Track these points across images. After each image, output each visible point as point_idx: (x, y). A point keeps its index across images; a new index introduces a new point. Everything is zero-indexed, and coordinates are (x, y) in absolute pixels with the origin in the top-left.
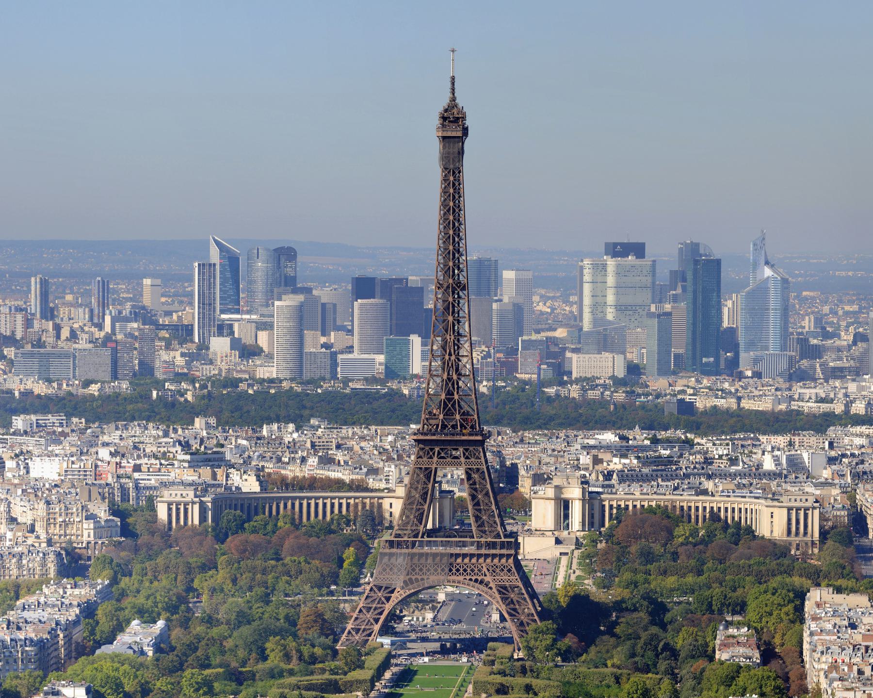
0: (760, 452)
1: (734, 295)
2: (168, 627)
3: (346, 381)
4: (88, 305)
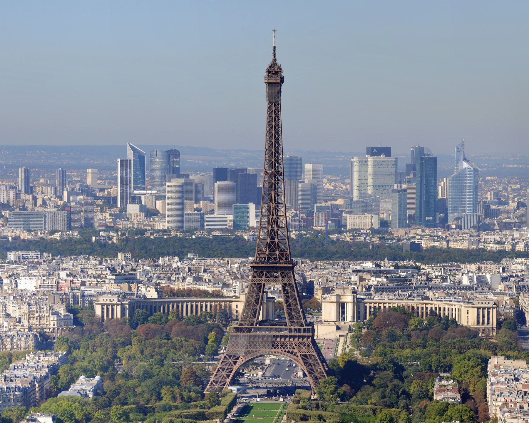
0: (461, 274)
1: (445, 179)
2: (102, 380)
3: (210, 231)
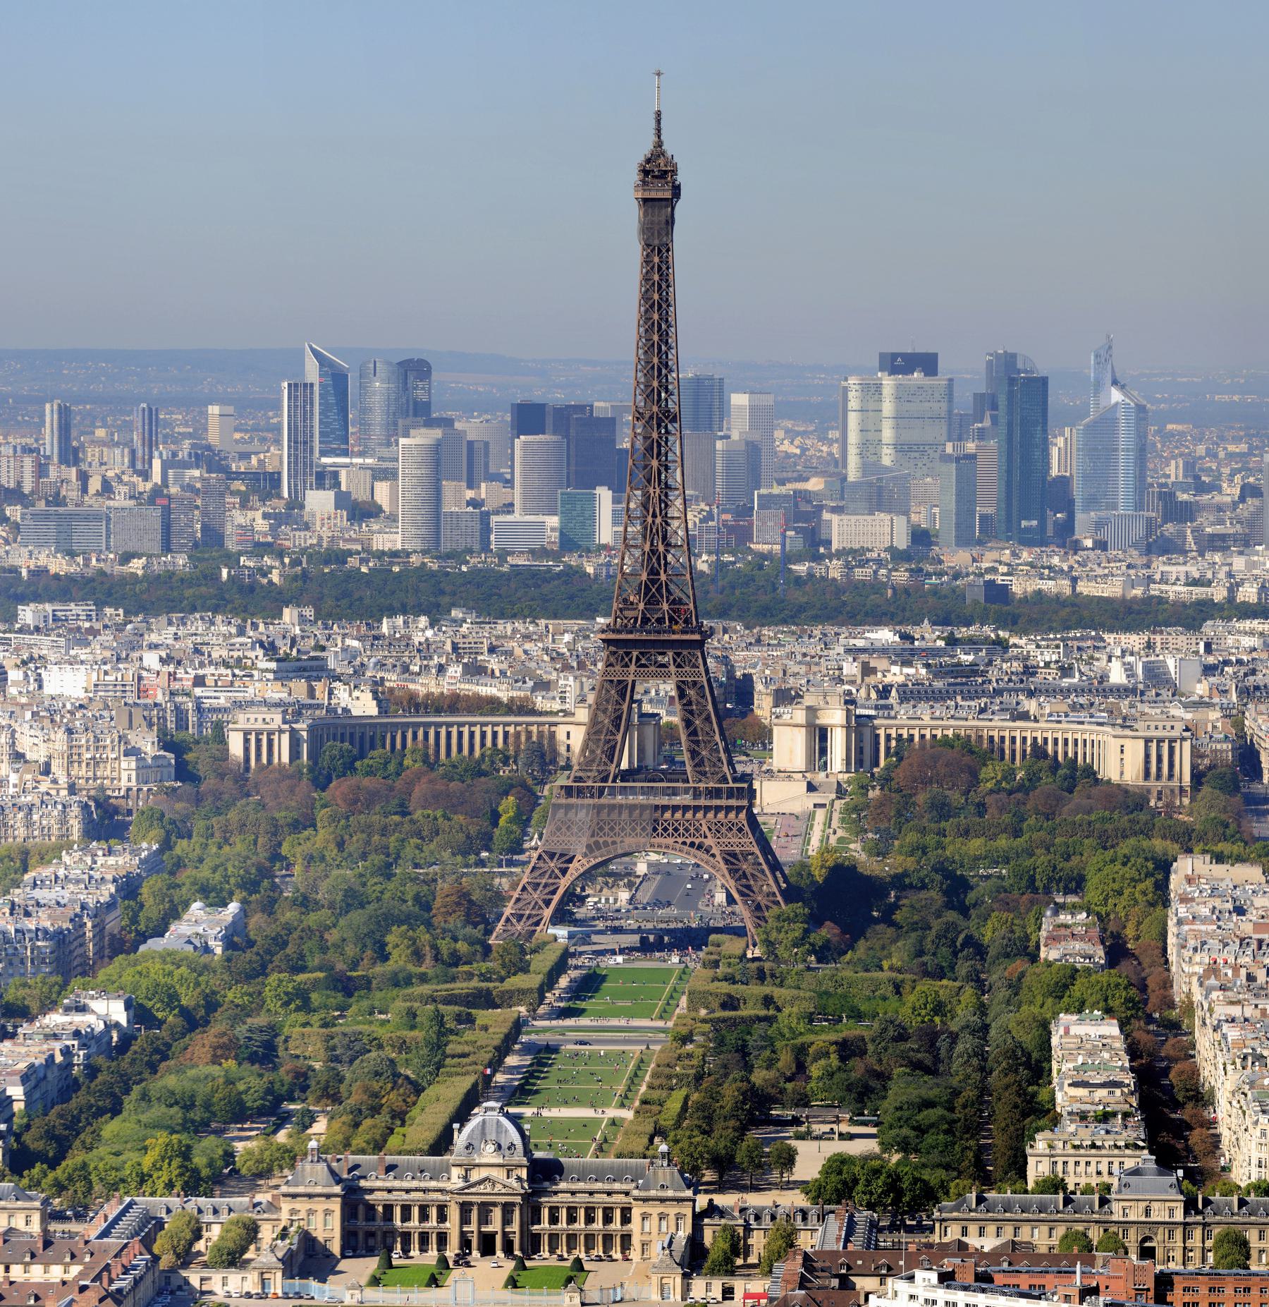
0: (1105, 657)
1: (1067, 430)
2: (244, 913)
3: (503, 555)
4: (128, 443)
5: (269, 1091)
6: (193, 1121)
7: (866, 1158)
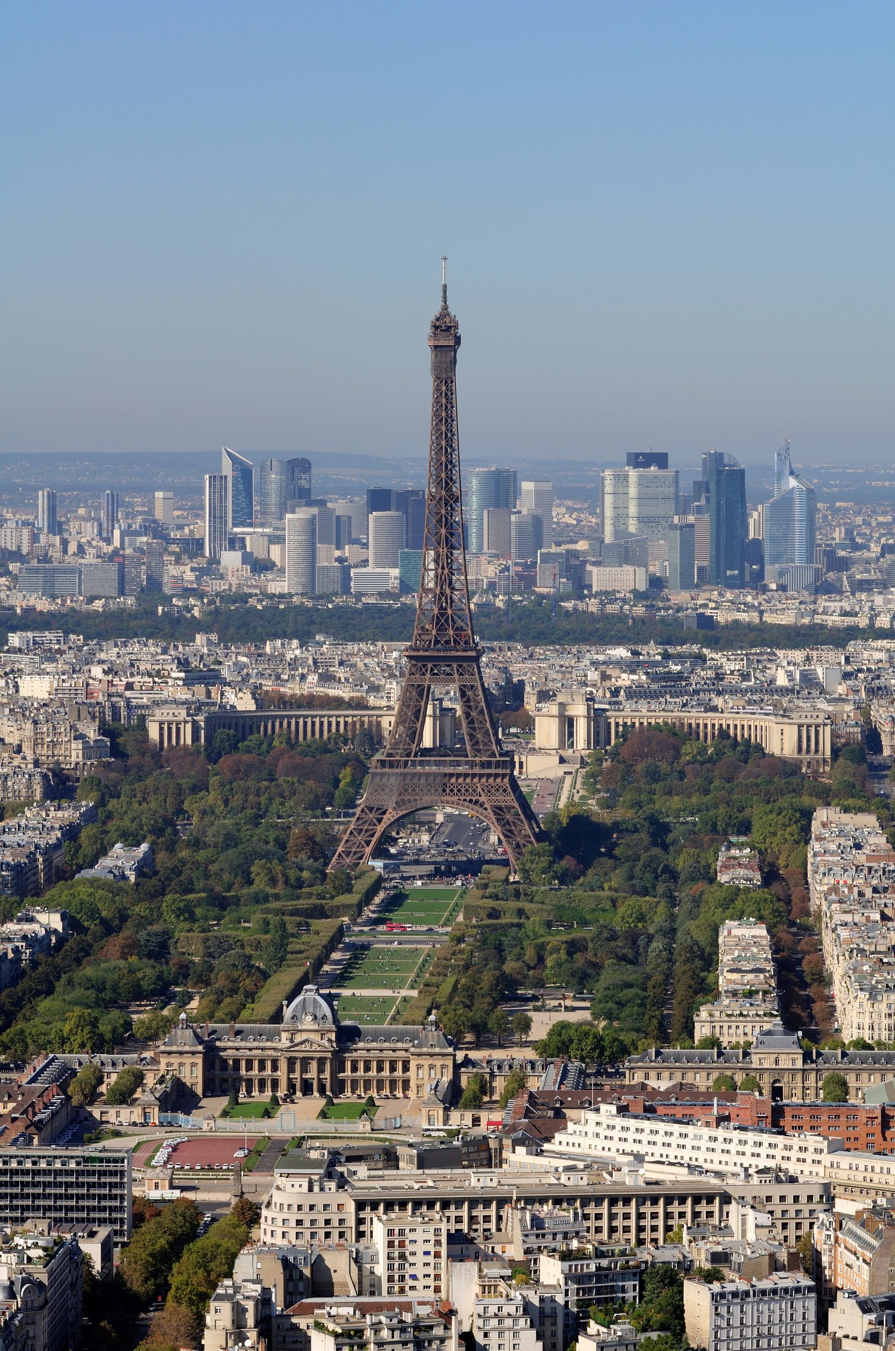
0: (774, 667)
2: (152, 850)
3: (359, 596)
5: (160, 977)
6: (103, 1000)
7: (580, 1024)
